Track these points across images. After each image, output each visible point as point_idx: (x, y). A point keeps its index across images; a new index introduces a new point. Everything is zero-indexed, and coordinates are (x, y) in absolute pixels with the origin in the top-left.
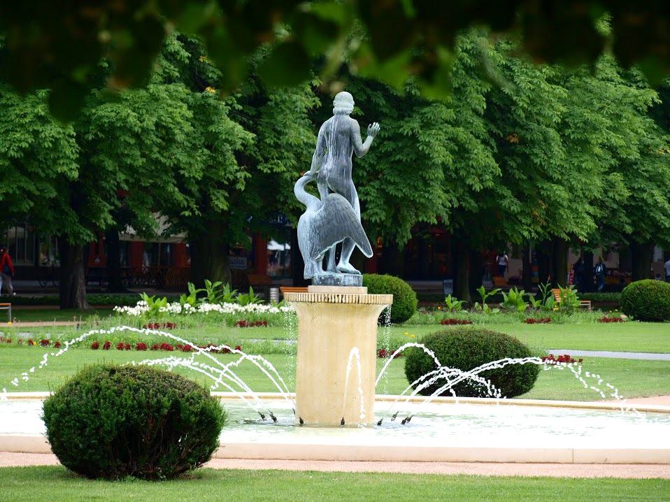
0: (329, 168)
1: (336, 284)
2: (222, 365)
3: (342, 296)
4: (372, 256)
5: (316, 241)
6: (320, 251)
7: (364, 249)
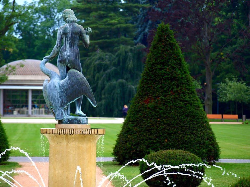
0: (68, 54)
1: (79, 123)
2: (7, 175)
3: (90, 130)
4: (96, 106)
5: (65, 98)
6: (66, 103)
7: (93, 102)
